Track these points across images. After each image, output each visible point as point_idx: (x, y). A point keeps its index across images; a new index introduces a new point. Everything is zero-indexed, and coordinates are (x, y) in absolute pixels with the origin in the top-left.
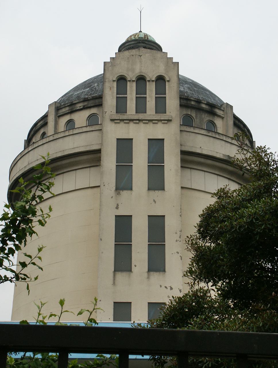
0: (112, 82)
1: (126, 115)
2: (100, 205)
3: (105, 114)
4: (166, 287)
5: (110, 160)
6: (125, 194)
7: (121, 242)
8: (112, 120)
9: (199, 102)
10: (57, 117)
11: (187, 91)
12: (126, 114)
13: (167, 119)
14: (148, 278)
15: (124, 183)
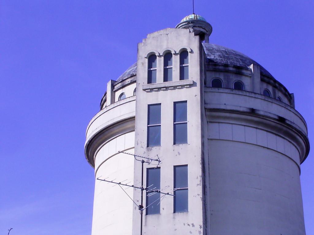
1: (155, 84)
4: (188, 225)
5: (142, 124)
8: (144, 90)
9: (226, 65)
11: (217, 58)
13: (189, 84)
14: (174, 218)
15: (153, 139)
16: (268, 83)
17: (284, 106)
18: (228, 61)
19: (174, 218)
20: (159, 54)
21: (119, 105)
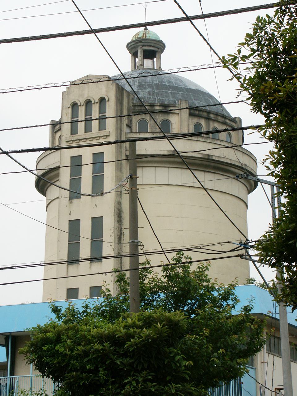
0: (68, 109)
2: (59, 214)
3: (63, 137)
6: (76, 201)
7: (74, 241)
10: (54, 133)
11: (146, 96)
12: (77, 135)
13: (106, 135)
14: (90, 268)
15: (75, 193)
16: (199, 116)
17: (212, 142)
18: (156, 98)
19: (90, 268)
20: (81, 104)
21: (49, 153)
